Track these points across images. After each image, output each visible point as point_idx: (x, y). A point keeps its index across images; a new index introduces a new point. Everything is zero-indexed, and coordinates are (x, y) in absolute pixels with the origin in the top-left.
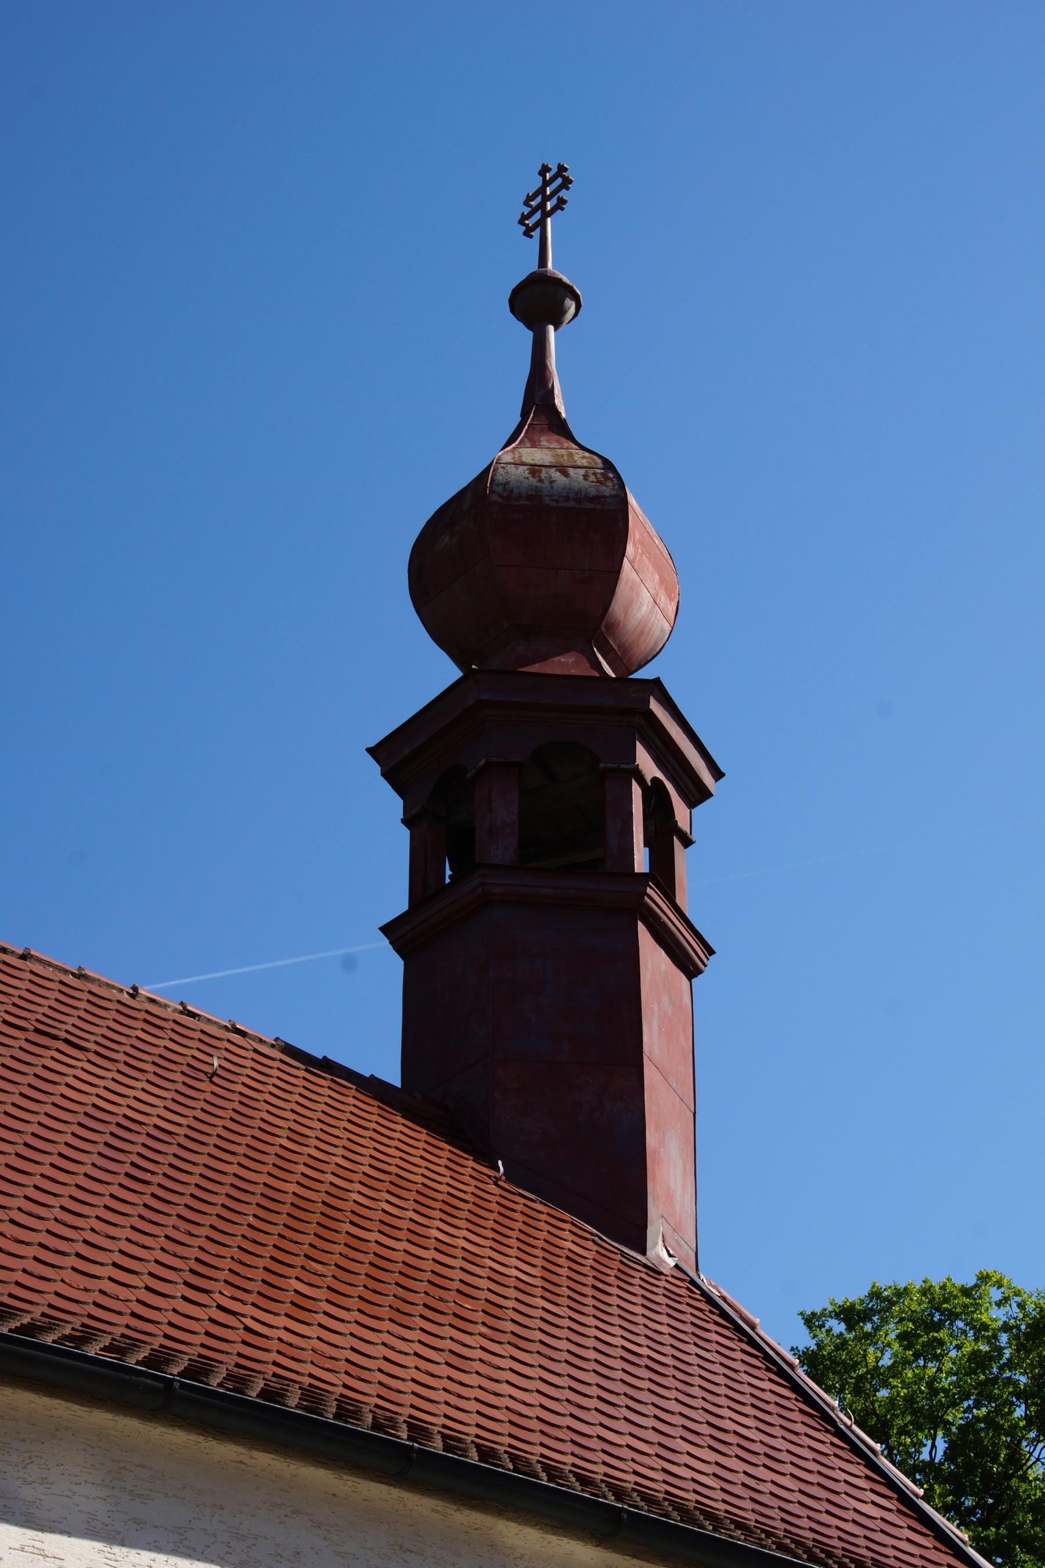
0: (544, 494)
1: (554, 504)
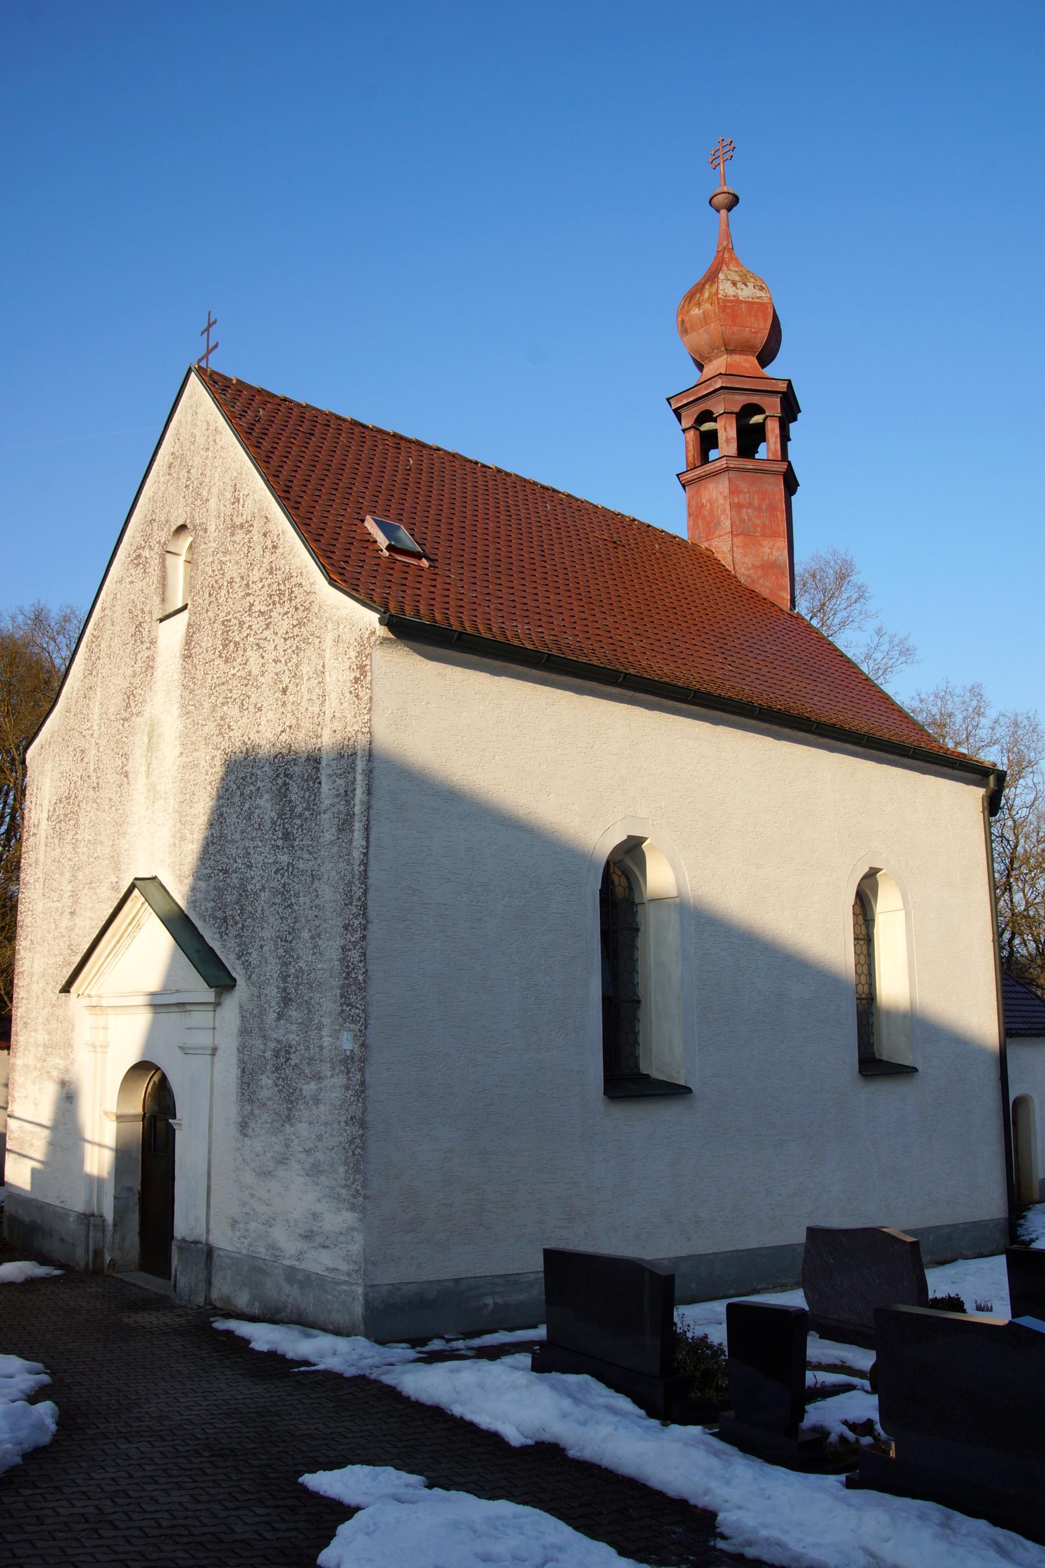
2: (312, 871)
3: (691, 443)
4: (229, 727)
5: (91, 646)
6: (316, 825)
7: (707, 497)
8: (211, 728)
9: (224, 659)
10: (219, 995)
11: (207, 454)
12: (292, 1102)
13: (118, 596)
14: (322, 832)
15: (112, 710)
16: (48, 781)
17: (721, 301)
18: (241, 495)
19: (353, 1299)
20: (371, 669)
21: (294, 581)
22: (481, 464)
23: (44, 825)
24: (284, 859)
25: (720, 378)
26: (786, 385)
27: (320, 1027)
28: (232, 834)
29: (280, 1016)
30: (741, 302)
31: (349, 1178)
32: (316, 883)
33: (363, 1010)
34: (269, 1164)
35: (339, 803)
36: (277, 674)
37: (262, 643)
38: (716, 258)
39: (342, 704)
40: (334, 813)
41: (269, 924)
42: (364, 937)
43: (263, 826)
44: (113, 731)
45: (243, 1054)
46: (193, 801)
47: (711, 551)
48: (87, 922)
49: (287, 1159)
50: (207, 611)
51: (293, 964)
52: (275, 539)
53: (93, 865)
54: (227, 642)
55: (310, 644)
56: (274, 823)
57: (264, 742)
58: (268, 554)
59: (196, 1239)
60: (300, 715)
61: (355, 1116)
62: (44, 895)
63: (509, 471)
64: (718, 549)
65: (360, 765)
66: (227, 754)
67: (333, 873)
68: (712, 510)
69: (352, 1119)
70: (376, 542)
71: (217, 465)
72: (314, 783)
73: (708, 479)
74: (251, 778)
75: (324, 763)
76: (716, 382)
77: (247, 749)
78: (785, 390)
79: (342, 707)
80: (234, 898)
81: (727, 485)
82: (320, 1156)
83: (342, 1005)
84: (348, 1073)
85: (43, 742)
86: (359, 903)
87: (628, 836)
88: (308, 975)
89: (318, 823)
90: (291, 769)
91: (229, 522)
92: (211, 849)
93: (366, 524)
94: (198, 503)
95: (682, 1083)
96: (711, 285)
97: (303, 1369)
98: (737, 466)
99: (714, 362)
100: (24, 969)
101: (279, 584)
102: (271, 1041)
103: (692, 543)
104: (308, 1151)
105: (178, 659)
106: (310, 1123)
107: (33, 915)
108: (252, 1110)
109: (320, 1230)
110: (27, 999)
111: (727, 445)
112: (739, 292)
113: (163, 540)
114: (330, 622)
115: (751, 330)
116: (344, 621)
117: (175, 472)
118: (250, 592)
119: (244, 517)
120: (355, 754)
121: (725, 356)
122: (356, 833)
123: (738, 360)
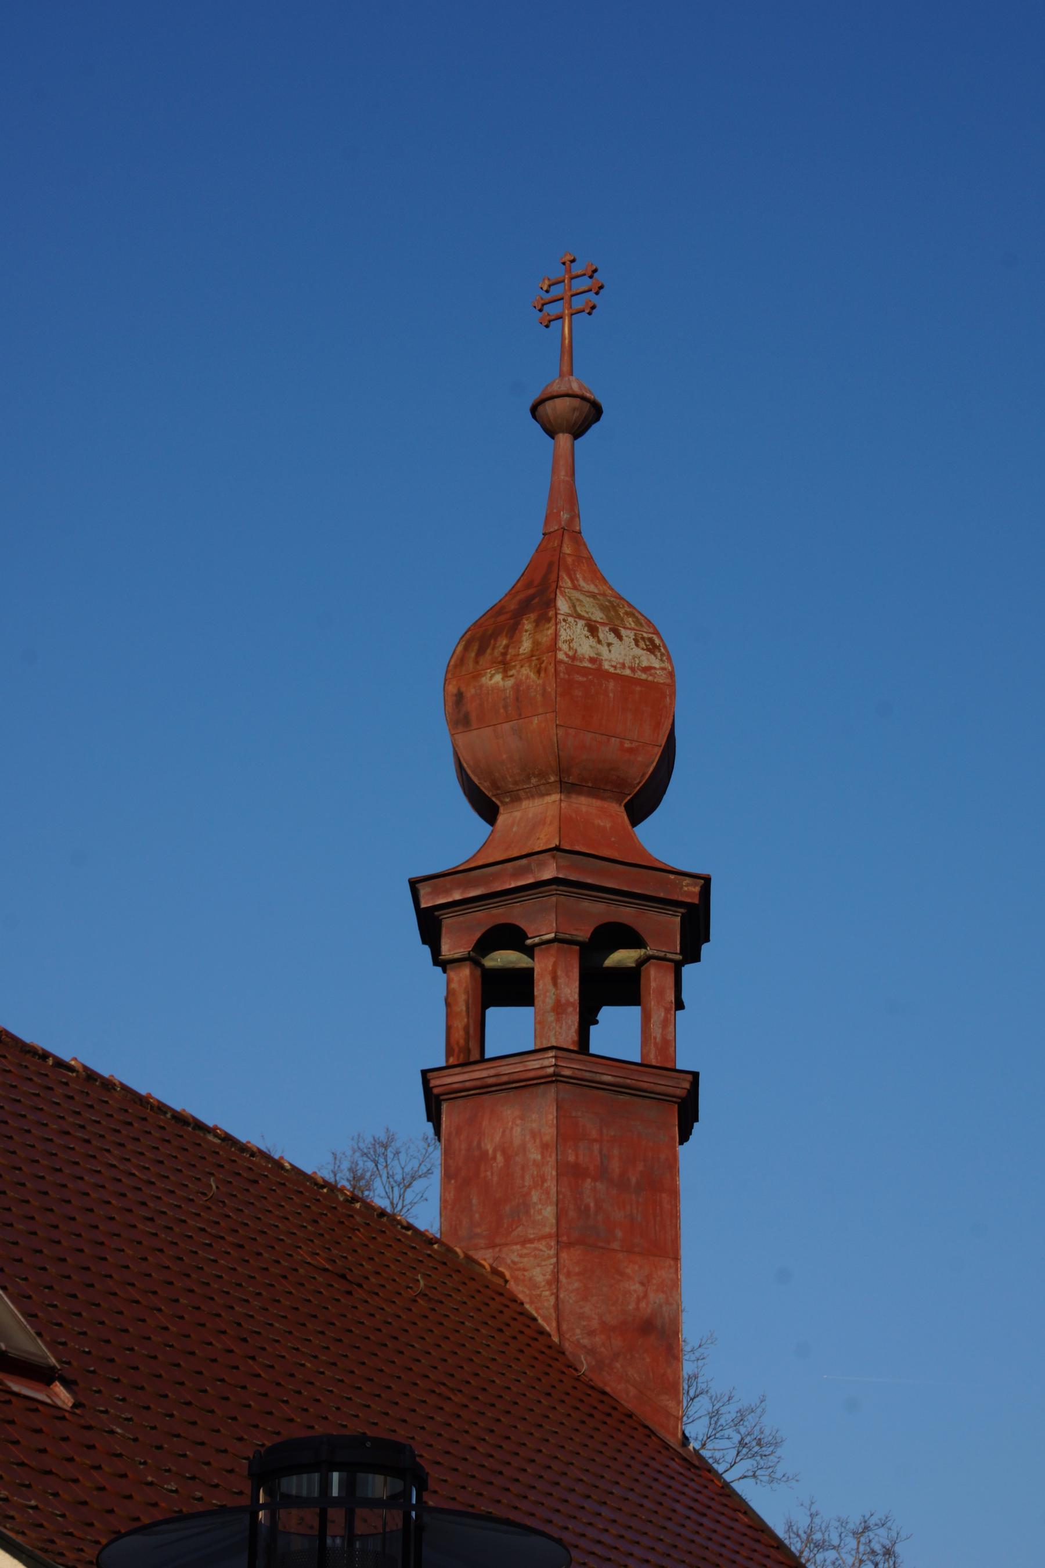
0: (603, 658)
1: (612, 670)
17: (562, 668)
22: (55, 1058)
25: (554, 857)
26: (697, 889)
30: (607, 675)
47: (501, 1275)
64: (519, 1273)
73: (503, 1094)
76: (542, 865)
78: (696, 901)
81: (552, 1116)
96: (538, 623)
98: (579, 1074)
99: (525, 804)
112: (604, 650)
115: (622, 744)
121: (556, 797)
123: (584, 809)
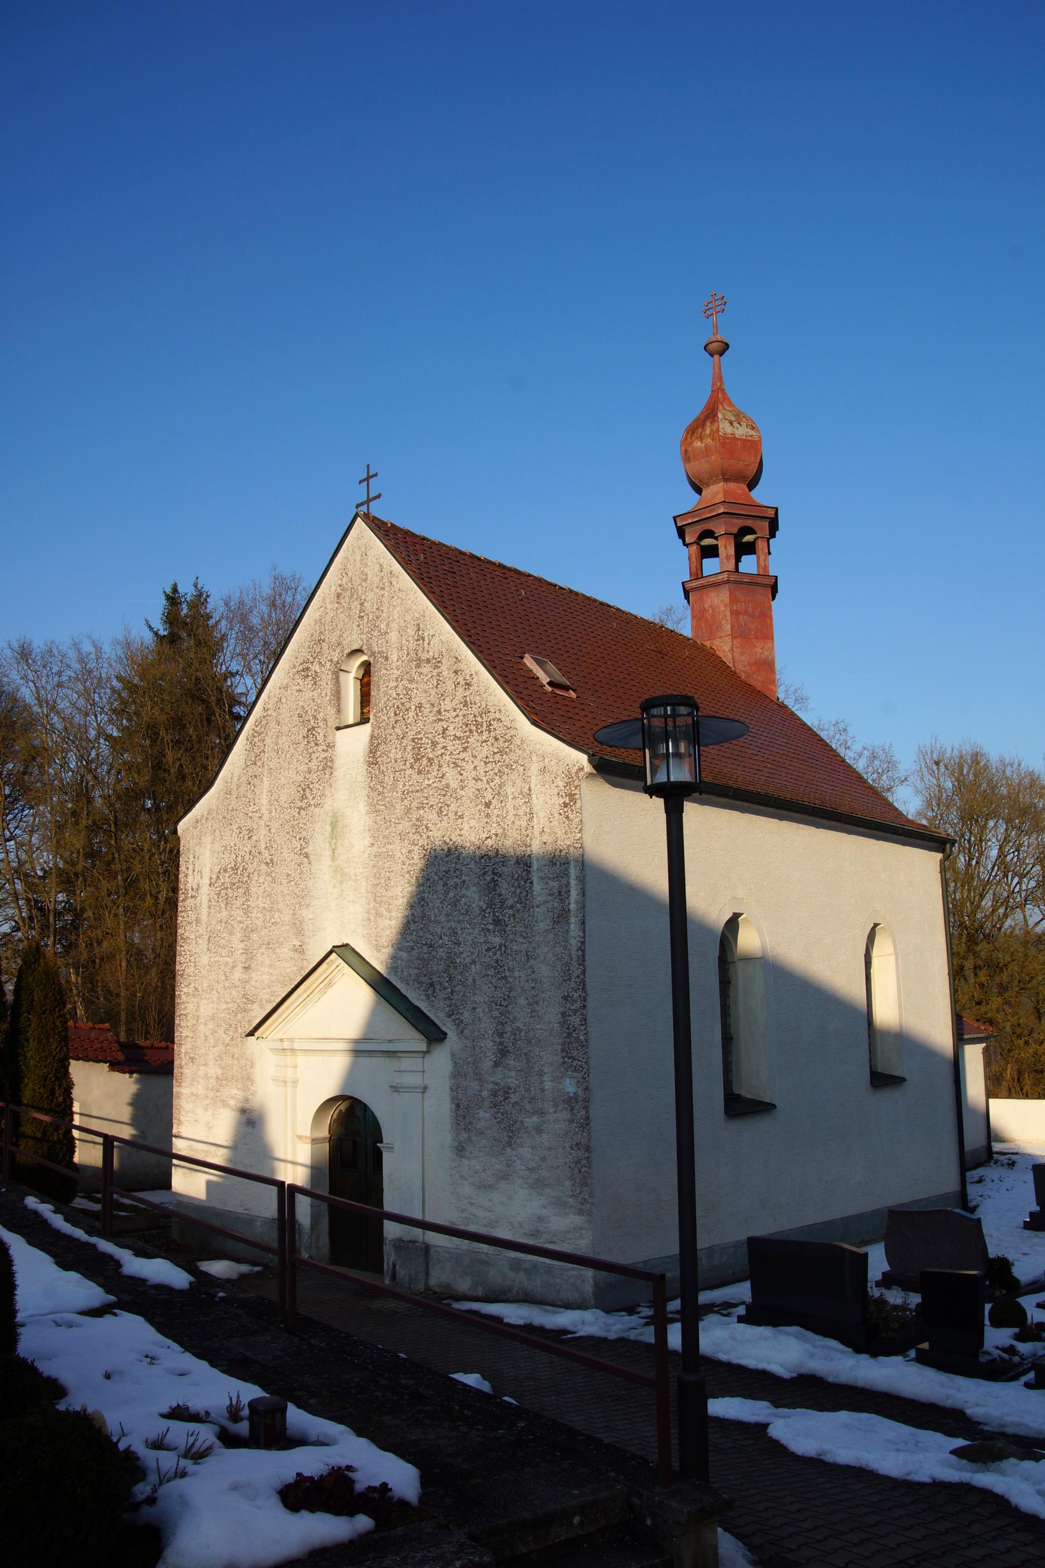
2: (526, 951)
3: (694, 556)
4: (427, 828)
5: (252, 740)
6: (529, 916)
7: (709, 603)
8: (405, 826)
9: (417, 770)
10: (429, 1045)
11: (382, 592)
12: (513, 1131)
13: (284, 700)
14: (537, 922)
15: (283, 798)
16: (208, 853)
17: (721, 438)
18: (426, 634)
19: (583, 1281)
20: (580, 798)
21: (492, 716)
23: (205, 889)
24: (497, 940)
26: (774, 512)
27: (541, 1074)
28: (436, 916)
29: (496, 1064)
30: (737, 439)
31: (576, 1190)
32: (532, 962)
33: (585, 1062)
34: (489, 1179)
35: (553, 900)
36: (478, 790)
37: (459, 763)
38: (711, 397)
39: (551, 822)
40: (548, 908)
41: (481, 990)
42: (584, 1007)
43: (471, 913)
44: (287, 817)
45: (457, 1092)
46: (389, 885)
47: (713, 649)
48: (266, 977)
49: (509, 1175)
50: (393, 728)
51: (509, 1023)
52: (468, 677)
53: (271, 929)
54: (419, 757)
55: (514, 770)
56: (482, 910)
57: (468, 845)
58: (460, 689)
59: (413, 1239)
60: (506, 826)
61: (580, 1143)
62: (208, 950)
63: (562, 586)
65: (573, 873)
66: (426, 850)
67: (550, 955)
68: (713, 616)
69: (577, 1145)
70: (538, 678)
71: (395, 604)
72: (526, 882)
73: (710, 589)
74: (455, 872)
75: (535, 867)
76: (719, 508)
77: (449, 848)
79: (552, 824)
80: (441, 967)
81: (728, 594)
82: (544, 1173)
83: (563, 1058)
84: (572, 1109)
85: (199, 817)
86: (578, 980)
87: (734, 913)
88: (526, 1033)
89: (531, 914)
90: (499, 869)
91: (413, 654)
92: (412, 927)
93: (525, 660)
94: (376, 633)
95: (768, 1100)
96: (711, 423)
97: (569, 1336)
99: (711, 487)
100: (187, 1012)
101: (475, 716)
102: (488, 1083)
103: (702, 644)
104: (531, 1170)
105: (362, 765)
106: (533, 1148)
107: (196, 966)
108: (469, 1137)
109: (546, 1230)
110: (192, 1038)
111: (728, 561)
113: (335, 660)
114: (534, 755)
116: (550, 756)
117: (345, 602)
118: (443, 718)
119: (431, 654)
120: (568, 863)
121: (722, 484)
122: (572, 926)
123: (732, 487)
